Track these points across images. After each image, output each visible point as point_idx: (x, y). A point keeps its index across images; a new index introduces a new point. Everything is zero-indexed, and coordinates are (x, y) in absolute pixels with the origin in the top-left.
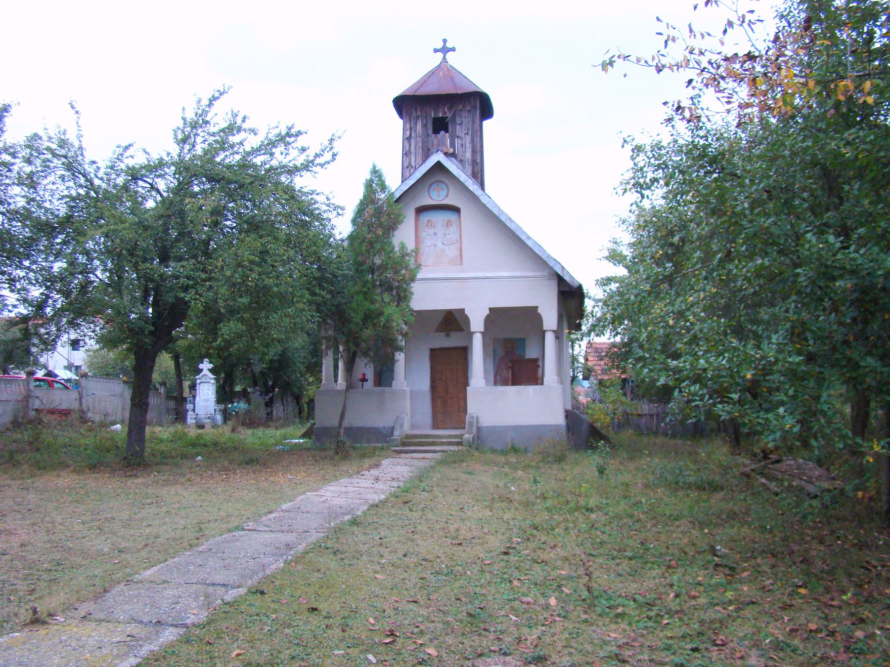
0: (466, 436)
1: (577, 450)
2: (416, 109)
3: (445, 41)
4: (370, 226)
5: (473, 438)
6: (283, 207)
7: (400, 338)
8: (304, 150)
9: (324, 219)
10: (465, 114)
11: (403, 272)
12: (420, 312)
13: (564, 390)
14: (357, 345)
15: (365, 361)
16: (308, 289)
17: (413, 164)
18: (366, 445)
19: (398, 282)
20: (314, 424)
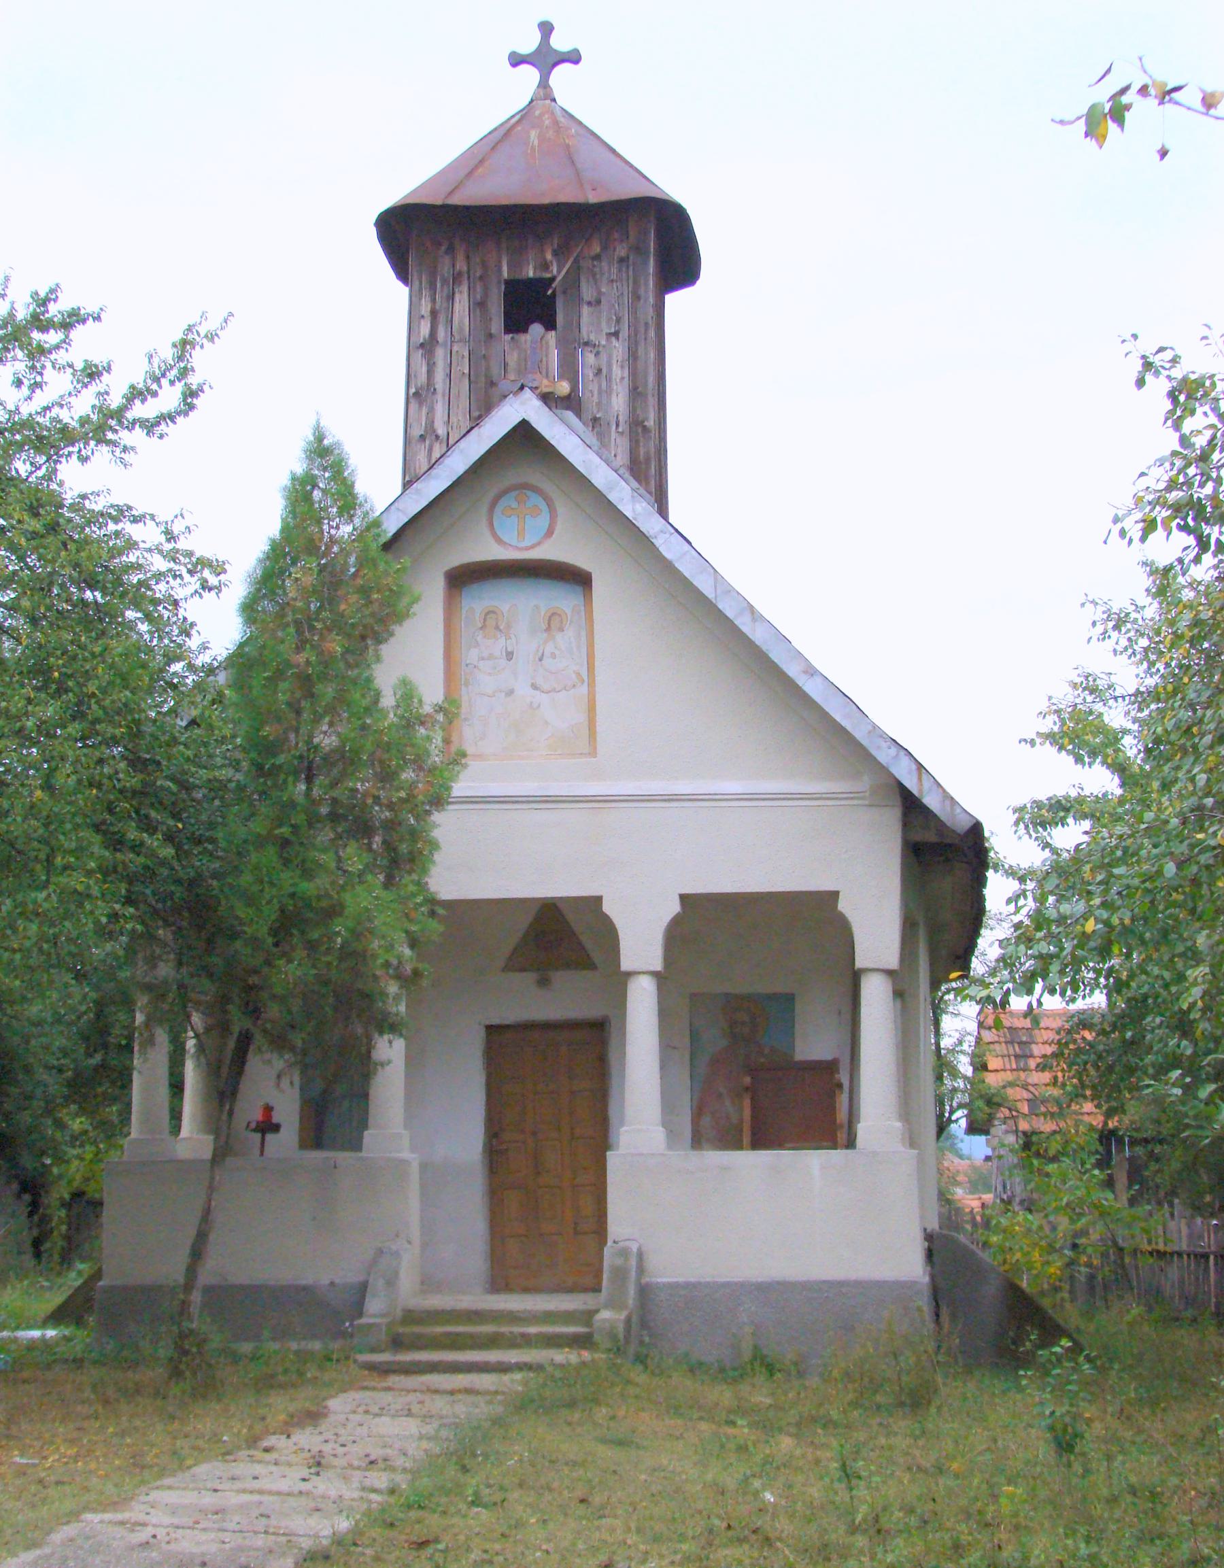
0: (605, 1314)
1: (968, 1371)
2: (451, 250)
3: (546, 29)
4: (304, 626)
5: (628, 1321)
6: (22, 558)
7: (393, 988)
8: (92, 373)
9: (156, 602)
10: (607, 269)
11: (408, 775)
12: (454, 906)
13: (921, 1160)
14: (255, 1012)
15: (279, 1064)
16: (97, 828)
17: (441, 431)
18: (274, 1346)
19: (390, 806)
20: (97, 1275)
